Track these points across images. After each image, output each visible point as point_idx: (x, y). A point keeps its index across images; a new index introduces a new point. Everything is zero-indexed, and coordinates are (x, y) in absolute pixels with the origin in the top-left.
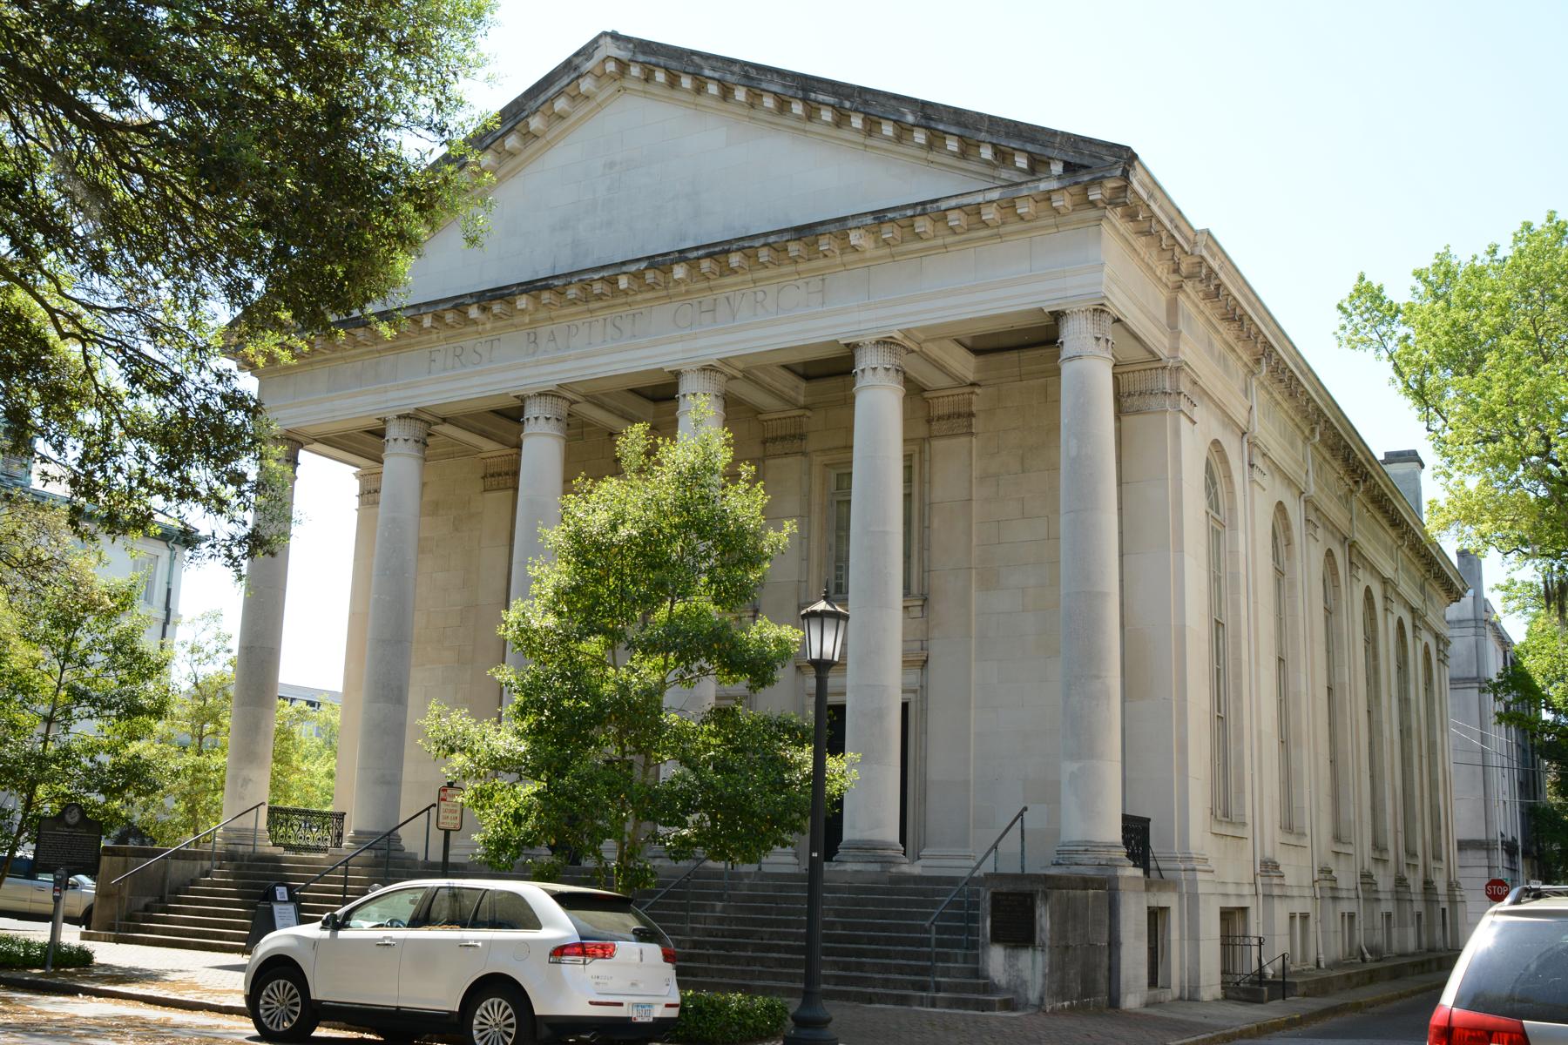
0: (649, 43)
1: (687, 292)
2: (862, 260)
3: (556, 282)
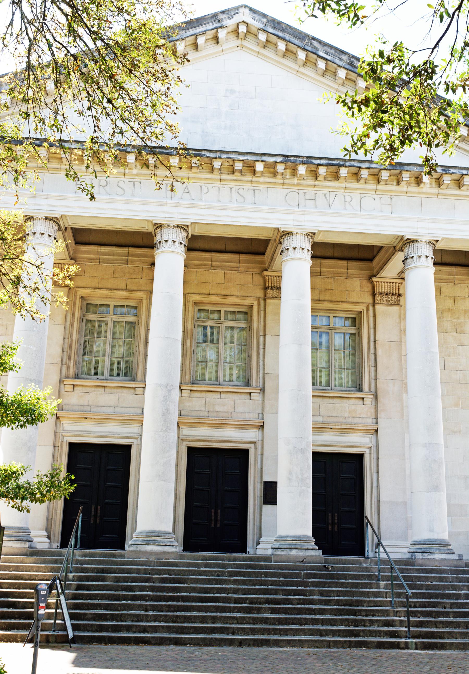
0: (279, 23)
1: (298, 185)
2: (419, 193)
3: (208, 154)
